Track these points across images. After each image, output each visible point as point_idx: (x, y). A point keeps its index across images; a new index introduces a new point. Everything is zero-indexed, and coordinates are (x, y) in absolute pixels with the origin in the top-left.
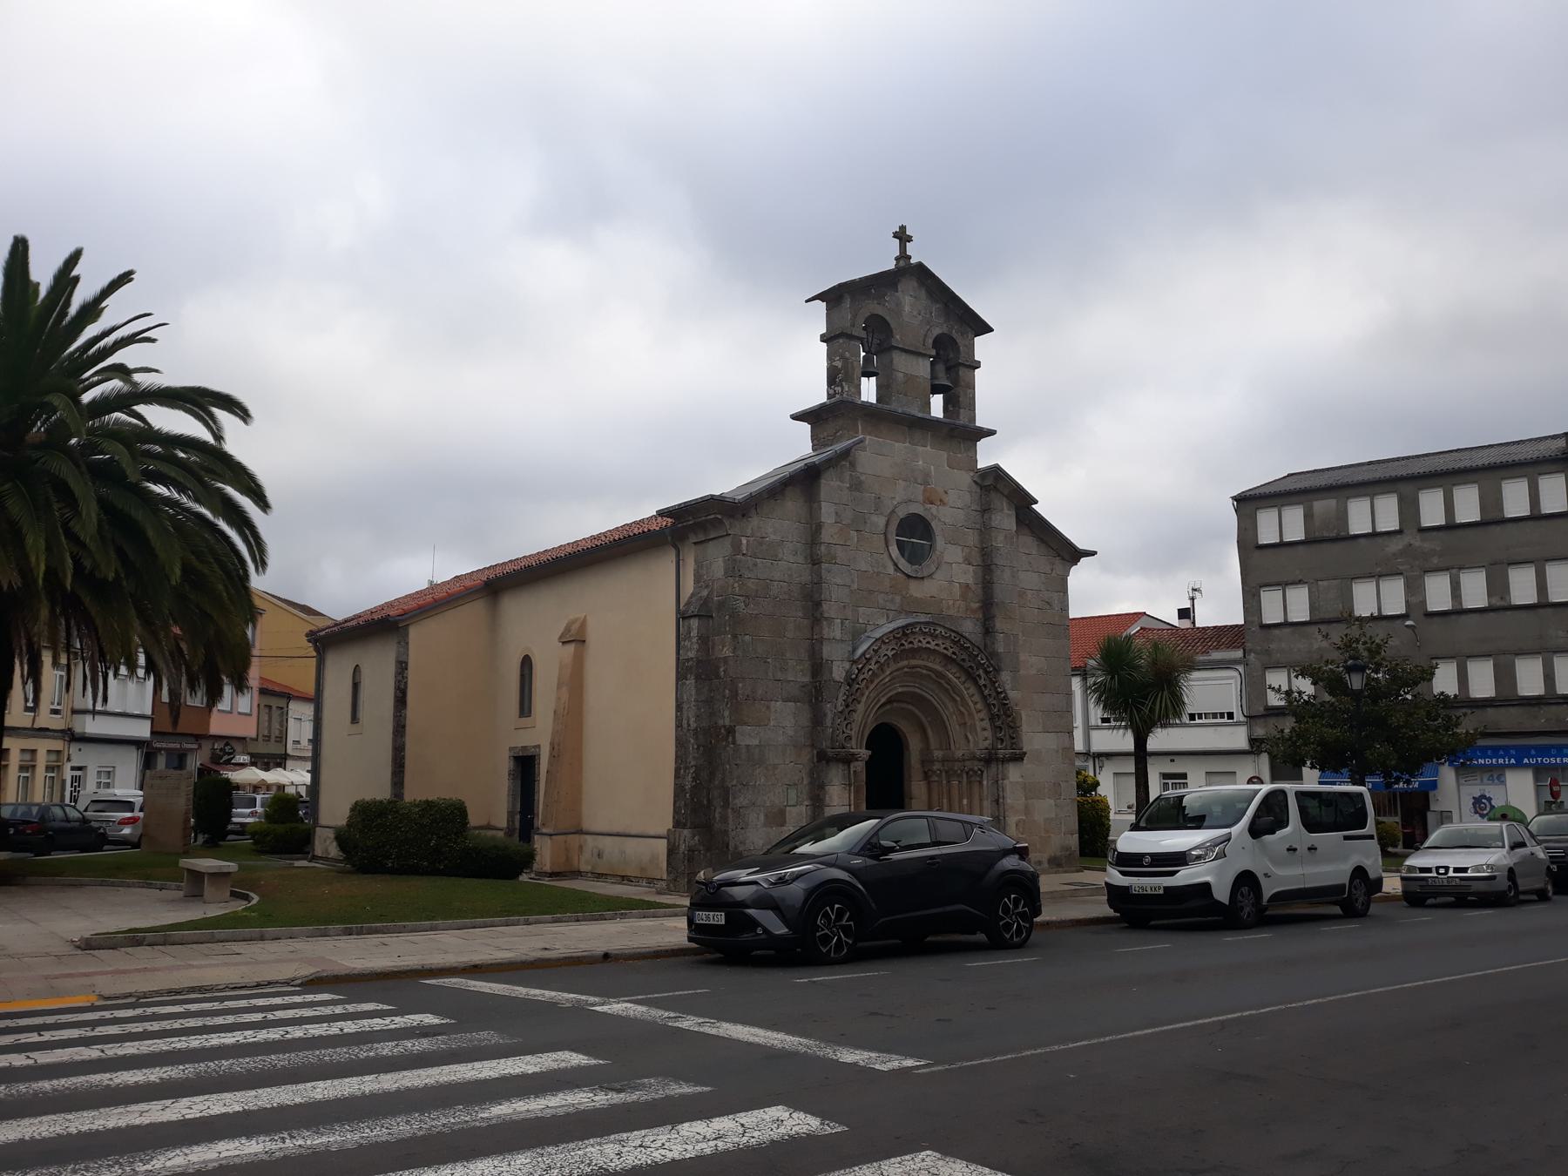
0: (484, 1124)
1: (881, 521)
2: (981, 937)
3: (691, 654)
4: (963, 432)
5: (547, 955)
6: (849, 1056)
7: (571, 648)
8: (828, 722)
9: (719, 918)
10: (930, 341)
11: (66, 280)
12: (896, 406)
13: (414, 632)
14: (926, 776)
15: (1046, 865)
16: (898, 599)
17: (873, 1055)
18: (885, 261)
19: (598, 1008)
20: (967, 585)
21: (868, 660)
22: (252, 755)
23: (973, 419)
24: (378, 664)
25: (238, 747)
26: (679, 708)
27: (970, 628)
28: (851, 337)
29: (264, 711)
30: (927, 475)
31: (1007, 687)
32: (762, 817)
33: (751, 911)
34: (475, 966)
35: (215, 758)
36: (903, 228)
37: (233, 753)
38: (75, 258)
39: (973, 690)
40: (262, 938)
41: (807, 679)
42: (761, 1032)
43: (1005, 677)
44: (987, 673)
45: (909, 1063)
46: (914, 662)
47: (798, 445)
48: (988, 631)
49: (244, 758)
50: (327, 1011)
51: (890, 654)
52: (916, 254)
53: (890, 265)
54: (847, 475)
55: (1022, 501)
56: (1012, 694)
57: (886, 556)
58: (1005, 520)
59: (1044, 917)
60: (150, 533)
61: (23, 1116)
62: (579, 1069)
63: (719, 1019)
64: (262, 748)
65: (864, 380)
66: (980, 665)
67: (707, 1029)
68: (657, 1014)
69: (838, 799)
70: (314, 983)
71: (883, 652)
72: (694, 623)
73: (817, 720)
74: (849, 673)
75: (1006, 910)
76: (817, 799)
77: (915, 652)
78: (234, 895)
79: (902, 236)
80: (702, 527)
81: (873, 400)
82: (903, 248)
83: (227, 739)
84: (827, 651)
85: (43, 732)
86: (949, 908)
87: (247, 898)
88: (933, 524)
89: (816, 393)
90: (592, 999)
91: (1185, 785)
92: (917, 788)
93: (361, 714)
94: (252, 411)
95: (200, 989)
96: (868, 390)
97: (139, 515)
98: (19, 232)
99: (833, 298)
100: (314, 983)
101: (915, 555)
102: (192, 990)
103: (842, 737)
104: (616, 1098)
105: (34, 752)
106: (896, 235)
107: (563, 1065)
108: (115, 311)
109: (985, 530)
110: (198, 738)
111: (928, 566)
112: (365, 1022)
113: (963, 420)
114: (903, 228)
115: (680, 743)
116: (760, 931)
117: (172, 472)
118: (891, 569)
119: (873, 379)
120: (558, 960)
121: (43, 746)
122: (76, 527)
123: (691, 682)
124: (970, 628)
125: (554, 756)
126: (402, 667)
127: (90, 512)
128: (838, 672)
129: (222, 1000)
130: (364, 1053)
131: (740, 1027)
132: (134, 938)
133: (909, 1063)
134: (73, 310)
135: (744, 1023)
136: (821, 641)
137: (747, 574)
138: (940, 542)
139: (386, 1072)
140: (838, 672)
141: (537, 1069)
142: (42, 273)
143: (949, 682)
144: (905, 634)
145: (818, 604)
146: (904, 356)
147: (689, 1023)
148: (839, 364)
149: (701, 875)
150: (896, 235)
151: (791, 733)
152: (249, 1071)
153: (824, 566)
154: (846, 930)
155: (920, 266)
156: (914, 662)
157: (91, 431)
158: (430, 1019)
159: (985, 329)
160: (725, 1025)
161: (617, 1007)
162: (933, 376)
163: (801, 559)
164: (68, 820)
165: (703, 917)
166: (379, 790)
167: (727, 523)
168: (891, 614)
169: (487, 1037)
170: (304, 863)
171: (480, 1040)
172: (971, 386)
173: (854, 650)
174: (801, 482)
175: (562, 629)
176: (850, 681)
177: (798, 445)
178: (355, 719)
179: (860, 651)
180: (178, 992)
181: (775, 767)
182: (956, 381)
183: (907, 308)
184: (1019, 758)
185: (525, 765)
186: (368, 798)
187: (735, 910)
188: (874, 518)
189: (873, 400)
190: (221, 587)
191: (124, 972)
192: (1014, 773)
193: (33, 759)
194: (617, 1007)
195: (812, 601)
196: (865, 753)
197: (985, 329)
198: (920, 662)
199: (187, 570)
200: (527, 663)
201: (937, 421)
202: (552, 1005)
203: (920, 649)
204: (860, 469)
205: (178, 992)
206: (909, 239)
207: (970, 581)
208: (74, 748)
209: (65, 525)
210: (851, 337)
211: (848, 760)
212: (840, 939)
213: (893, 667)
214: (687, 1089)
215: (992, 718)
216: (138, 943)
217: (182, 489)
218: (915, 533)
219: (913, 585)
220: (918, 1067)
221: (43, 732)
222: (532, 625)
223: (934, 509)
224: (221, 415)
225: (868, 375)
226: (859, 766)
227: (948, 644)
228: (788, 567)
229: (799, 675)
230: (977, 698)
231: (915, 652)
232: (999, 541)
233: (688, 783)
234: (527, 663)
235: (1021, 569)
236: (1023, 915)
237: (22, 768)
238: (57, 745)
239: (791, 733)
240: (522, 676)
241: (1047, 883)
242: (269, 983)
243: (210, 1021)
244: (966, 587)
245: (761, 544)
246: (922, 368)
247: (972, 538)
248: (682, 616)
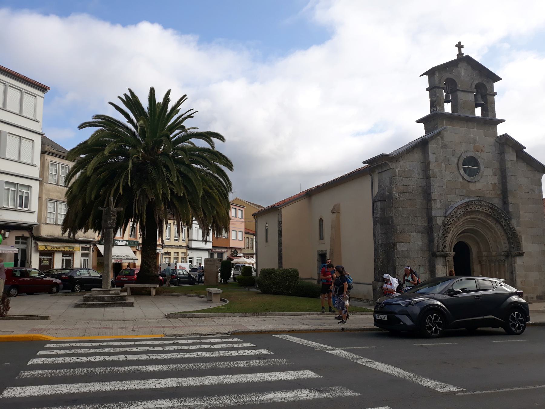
0: (259, 403)
1: (456, 160)
2: (501, 329)
3: (378, 216)
4: (490, 121)
5: (320, 328)
6: (427, 383)
7: (335, 215)
8: (436, 241)
9: (385, 318)
10: (474, 86)
11: (166, 100)
12: (460, 113)
13: (284, 211)
14: (480, 262)
15: (535, 299)
16: (464, 191)
17: (438, 383)
18: (453, 56)
19: (330, 352)
20: (495, 184)
21: (452, 216)
22: (243, 254)
23: (495, 116)
24: (271, 222)
25: (239, 251)
26: (374, 236)
28: (439, 88)
29: (247, 239)
31: (515, 225)
33: (397, 316)
34: (293, 331)
35: (232, 255)
36: (459, 43)
37: (237, 253)
38: (168, 93)
39: (499, 227)
40: (225, 316)
41: (426, 224)
42: (391, 367)
43: (514, 222)
44: (506, 220)
45: (454, 389)
46: (472, 216)
47: (420, 131)
48: (505, 202)
49: (241, 255)
50: (236, 346)
51: (462, 213)
52: (465, 52)
53: (455, 57)
54: (440, 142)
55: (518, 148)
56: (517, 228)
57: (458, 174)
58: (511, 156)
59: (530, 322)
60: (193, 180)
61: (106, 381)
62: (310, 380)
63: (376, 360)
64: (246, 251)
65: (446, 104)
66: (502, 217)
67: (369, 365)
68: (352, 356)
69: (441, 271)
70: (235, 334)
71: (459, 212)
72: (379, 204)
73: (431, 241)
74: (444, 221)
75: (513, 319)
76: (432, 271)
77: (473, 212)
78: (222, 300)
79: (459, 46)
80: (380, 166)
81: (450, 111)
82: (460, 51)
83: (235, 249)
84: (434, 213)
85: (180, 247)
86: (485, 317)
87: (226, 302)
88: (479, 160)
89: (426, 111)
90: (329, 347)
92: (476, 267)
93: (268, 239)
94: (225, 138)
95: (198, 334)
96: (448, 108)
97: (190, 175)
98: (151, 86)
99: (431, 73)
100: (235, 334)
101: (472, 173)
102: (195, 334)
103: (441, 247)
104: (318, 395)
105: (178, 253)
106: (457, 46)
107: (304, 377)
108: (183, 108)
109: (502, 161)
110: (226, 248)
111: (476, 178)
112: (241, 352)
113: (490, 117)
114: (459, 43)
115: (376, 250)
116: (402, 323)
117: (200, 160)
118: (461, 179)
119: (450, 104)
120: (324, 330)
121: (180, 251)
122: (171, 179)
123: (378, 226)
124: (497, 202)
125: (331, 254)
126: (280, 223)
127: (175, 174)
128: (439, 221)
129: (201, 339)
130: (233, 365)
131: (383, 365)
132: (184, 315)
133: (454, 389)
134: (169, 110)
135: (386, 363)
136: (431, 209)
137: (399, 184)
138: (482, 167)
139: (236, 374)
141: (293, 378)
142: (159, 99)
143: (488, 224)
144: (468, 205)
145: (430, 194)
146: (462, 93)
147: (363, 361)
148: (434, 99)
149: (378, 300)
150: (457, 46)
151: (420, 246)
152: (190, 369)
153: (431, 179)
154: (439, 325)
155: (468, 57)
156: (472, 216)
157: (177, 149)
158: (265, 352)
159: (498, 79)
160: (378, 363)
161: (337, 352)
162: (476, 99)
163: (421, 177)
164: (184, 274)
165: (379, 317)
166: (274, 265)
167: (390, 164)
168: (462, 197)
169: (283, 361)
170: (254, 290)
171: (278, 363)
172: (493, 103)
173: (446, 212)
174: (421, 145)
175: (332, 208)
176: (444, 224)
177: (420, 131)
178: (267, 241)
179: (448, 212)
180: (190, 335)
182: (486, 102)
183: (463, 74)
184: (522, 255)
185: (322, 256)
186: (266, 268)
187: (391, 315)
188: (453, 159)
189: (450, 111)
190: (217, 197)
191: (175, 327)
192: (519, 261)
193: (178, 255)
194: (337, 352)
195: (427, 194)
196: (453, 253)
197: (498, 79)
198: (475, 216)
199: (205, 191)
200: (321, 220)
201: (478, 118)
202: (313, 349)
203: (475, 211)
204: (445, 140)
205: (190, 335)
206: (463, 47)
207: (497, 182)
208: (189, 252)
209: (168, 179)
210: (439, 88)
211: (445, 256)
212: (436, 328)
213: (464, 218)
214: (349, 394)
215: (508, 239)
216: (185, 317)
217: (205, 166)
218: (471, 164)
219: (471, 185)
220: (458, 392)
221: (180, 247)
222: (323, 206)
223: (479, 154)
224: (213, 139)
225: (447, 102)
226: (451, 259)
227: (487, 208)
228: (415, 181)
229: (422, 222)
230: (501, 230)
231: (473, 212)
232: (508, 165)
233: (379, 264)
234: (321, 220)
235: (519, 176)
236: (521, 321)
237: (175, 258)
238: (184, 251)
239: (420, 246)
240: (320, 225)
241: (531, 307)
242: (221, 333)
243: (191, 347)
244: (494, 185)
245: (404, 171)
246: (471, 97)
247: (497, 165)
248: (374, 201)
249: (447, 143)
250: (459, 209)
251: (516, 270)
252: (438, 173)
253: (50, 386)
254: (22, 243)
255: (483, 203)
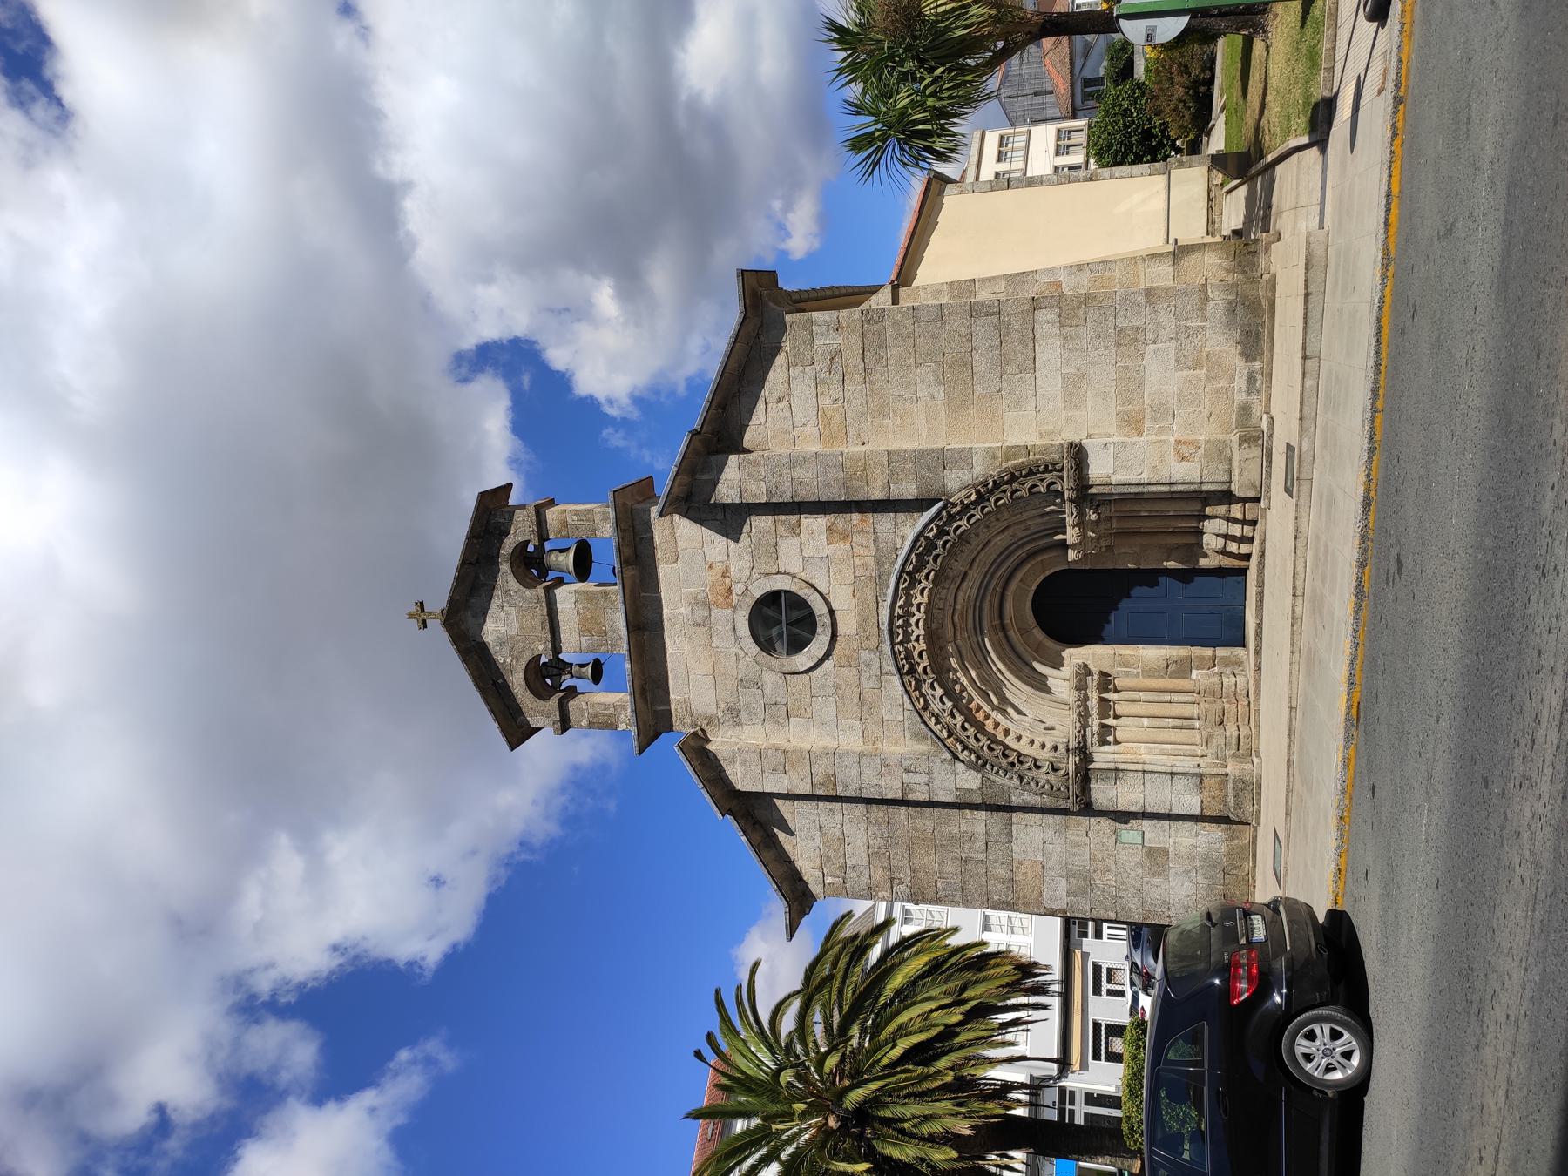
27: (910, 527)
30: (695, 602)
32: (1158, 880)
57: (814, 674)
88: (758, 594)
91: (1072, 1093)
124: (910, 527)
128: (970, 780)
140: (970, 780)
176: (980, 765)
181: (1092, 858)
184: (1078, 454)
204: (712, 710)
223: (738, 589)
239: (1051, 832)
245: (829, 859)
249: (723, 706)
250: (925, 708)
251: (1133, 479)
252: (821, 768)
253: (1370, 983)
254: (1072, 1102)
255: (898, 611)
